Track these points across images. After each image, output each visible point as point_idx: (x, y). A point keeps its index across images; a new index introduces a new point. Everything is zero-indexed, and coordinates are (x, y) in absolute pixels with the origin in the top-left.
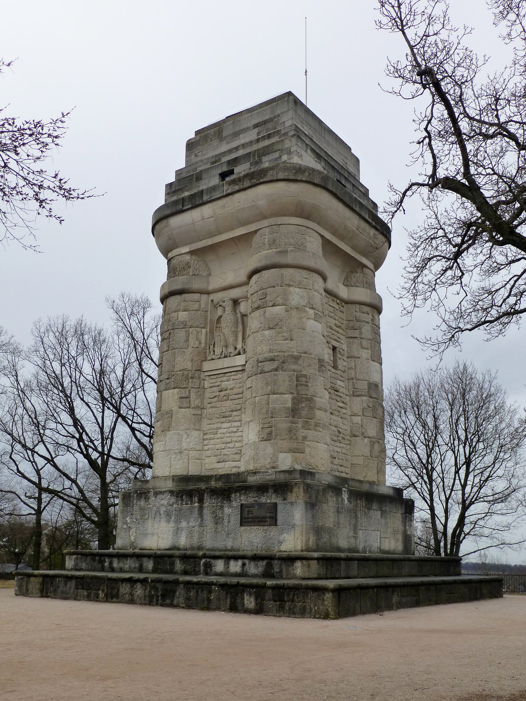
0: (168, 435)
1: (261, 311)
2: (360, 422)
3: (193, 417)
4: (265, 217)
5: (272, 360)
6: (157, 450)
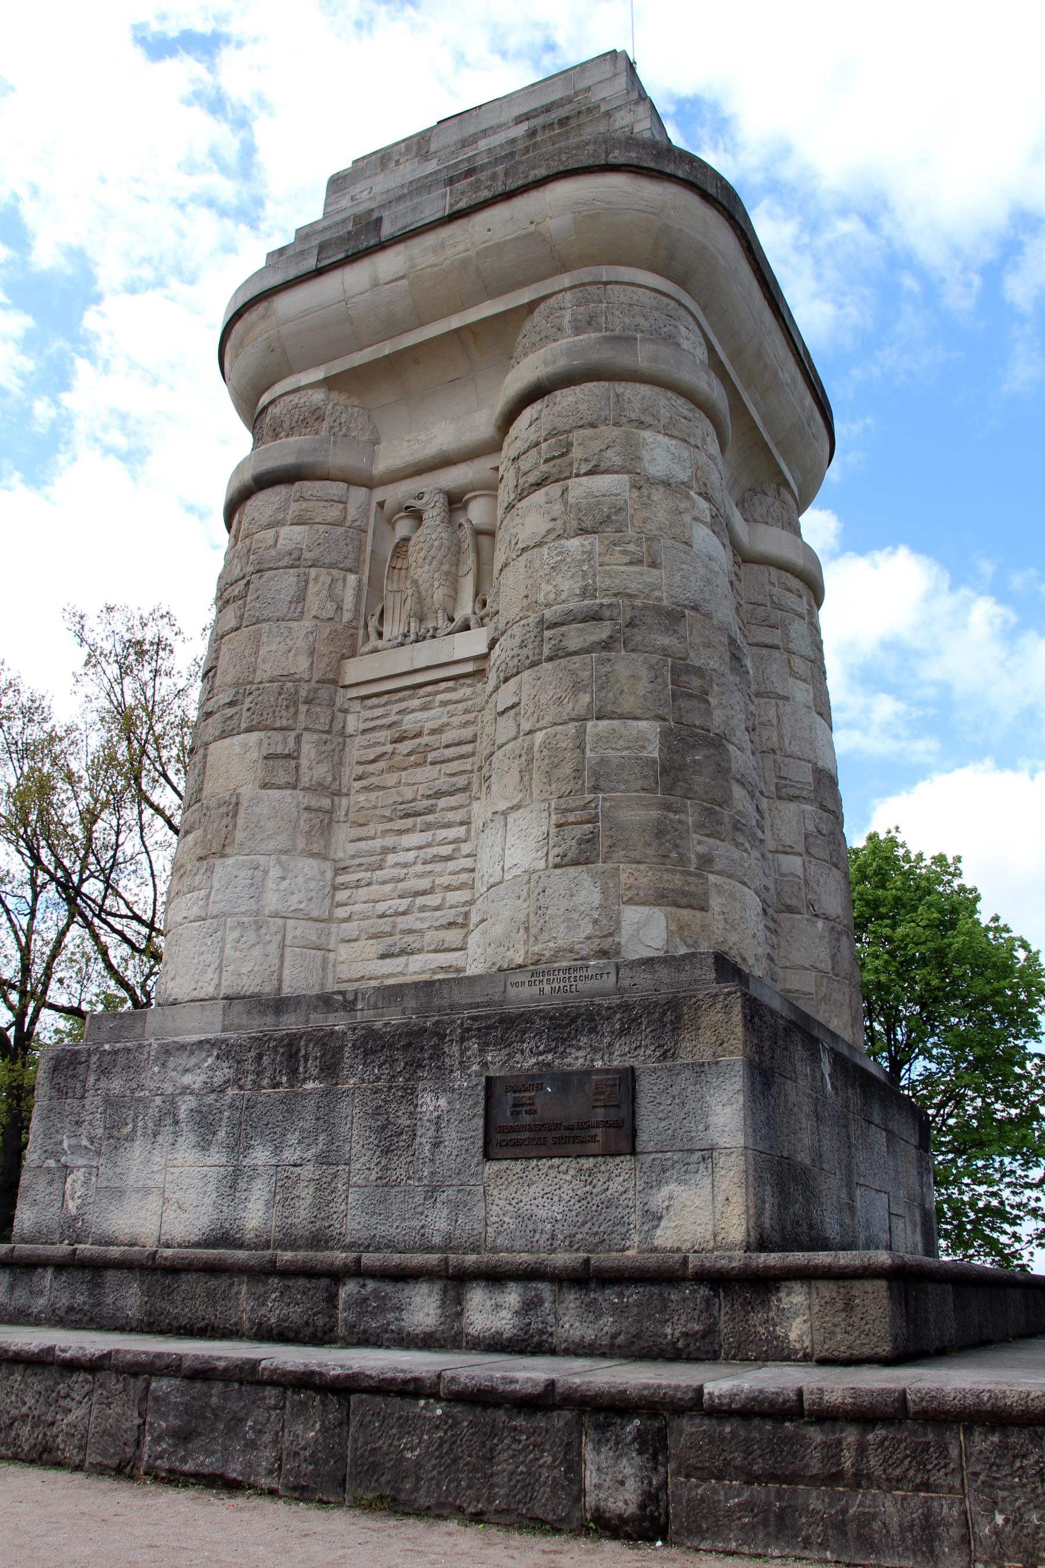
0: (218, 869)
1: (555, 490)
2: (800, 871)
3: (305, 815)
4: (564, 267)
5: (594, 617)
6: (179, 919)
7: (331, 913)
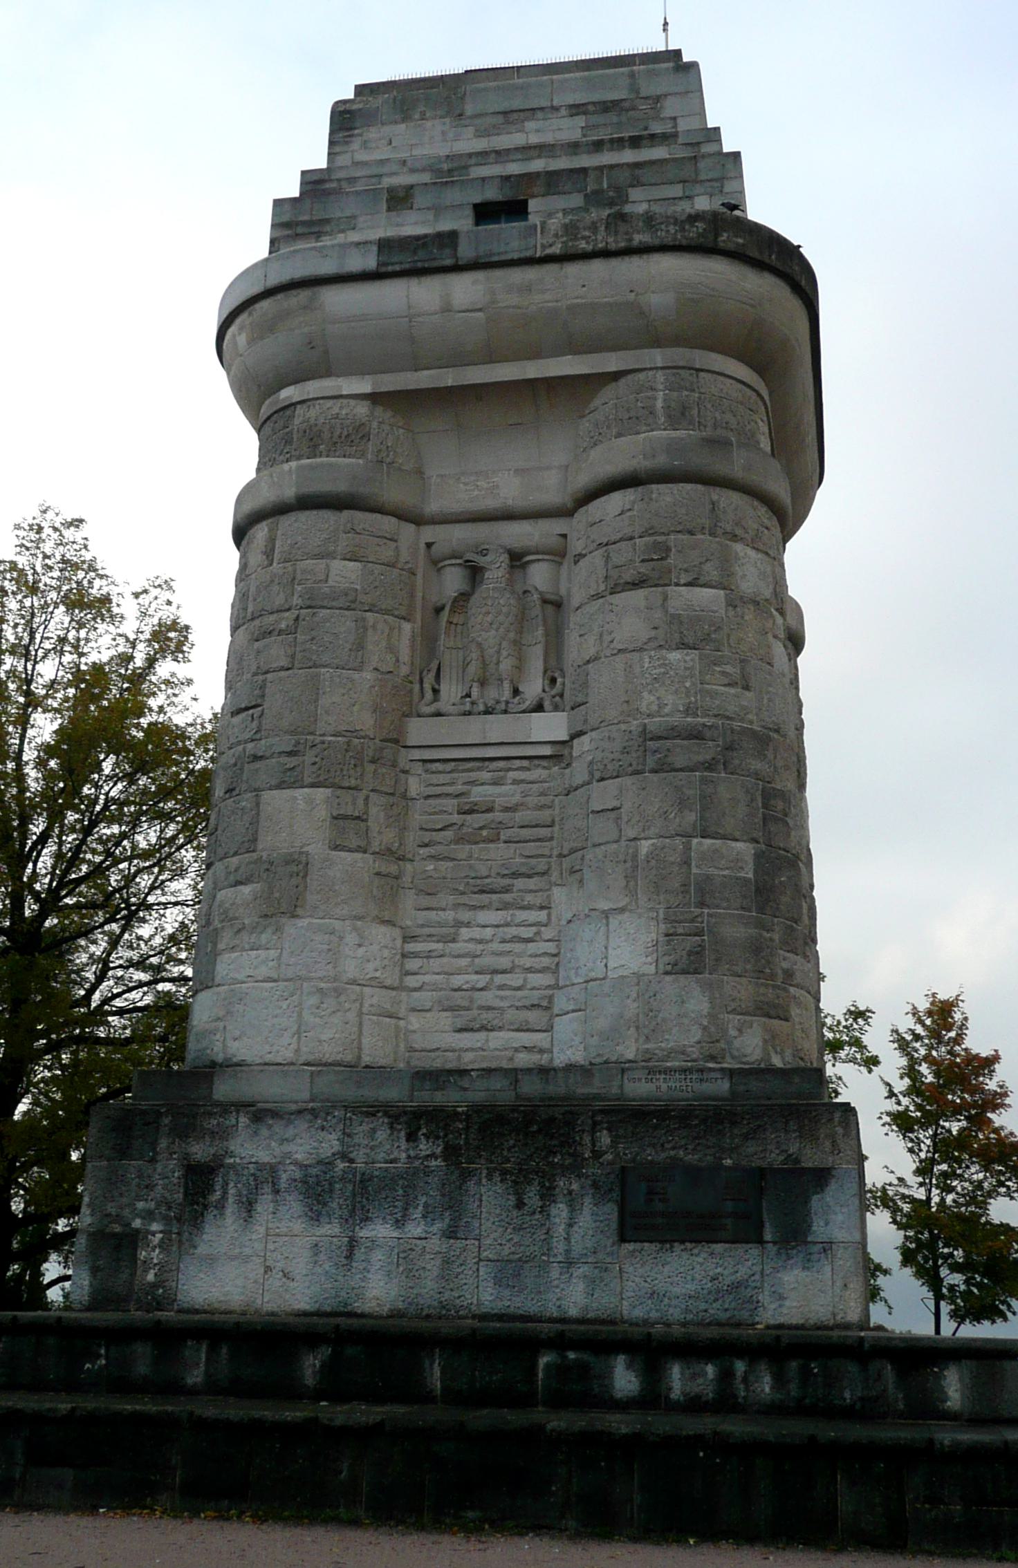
7: (401, 981)
